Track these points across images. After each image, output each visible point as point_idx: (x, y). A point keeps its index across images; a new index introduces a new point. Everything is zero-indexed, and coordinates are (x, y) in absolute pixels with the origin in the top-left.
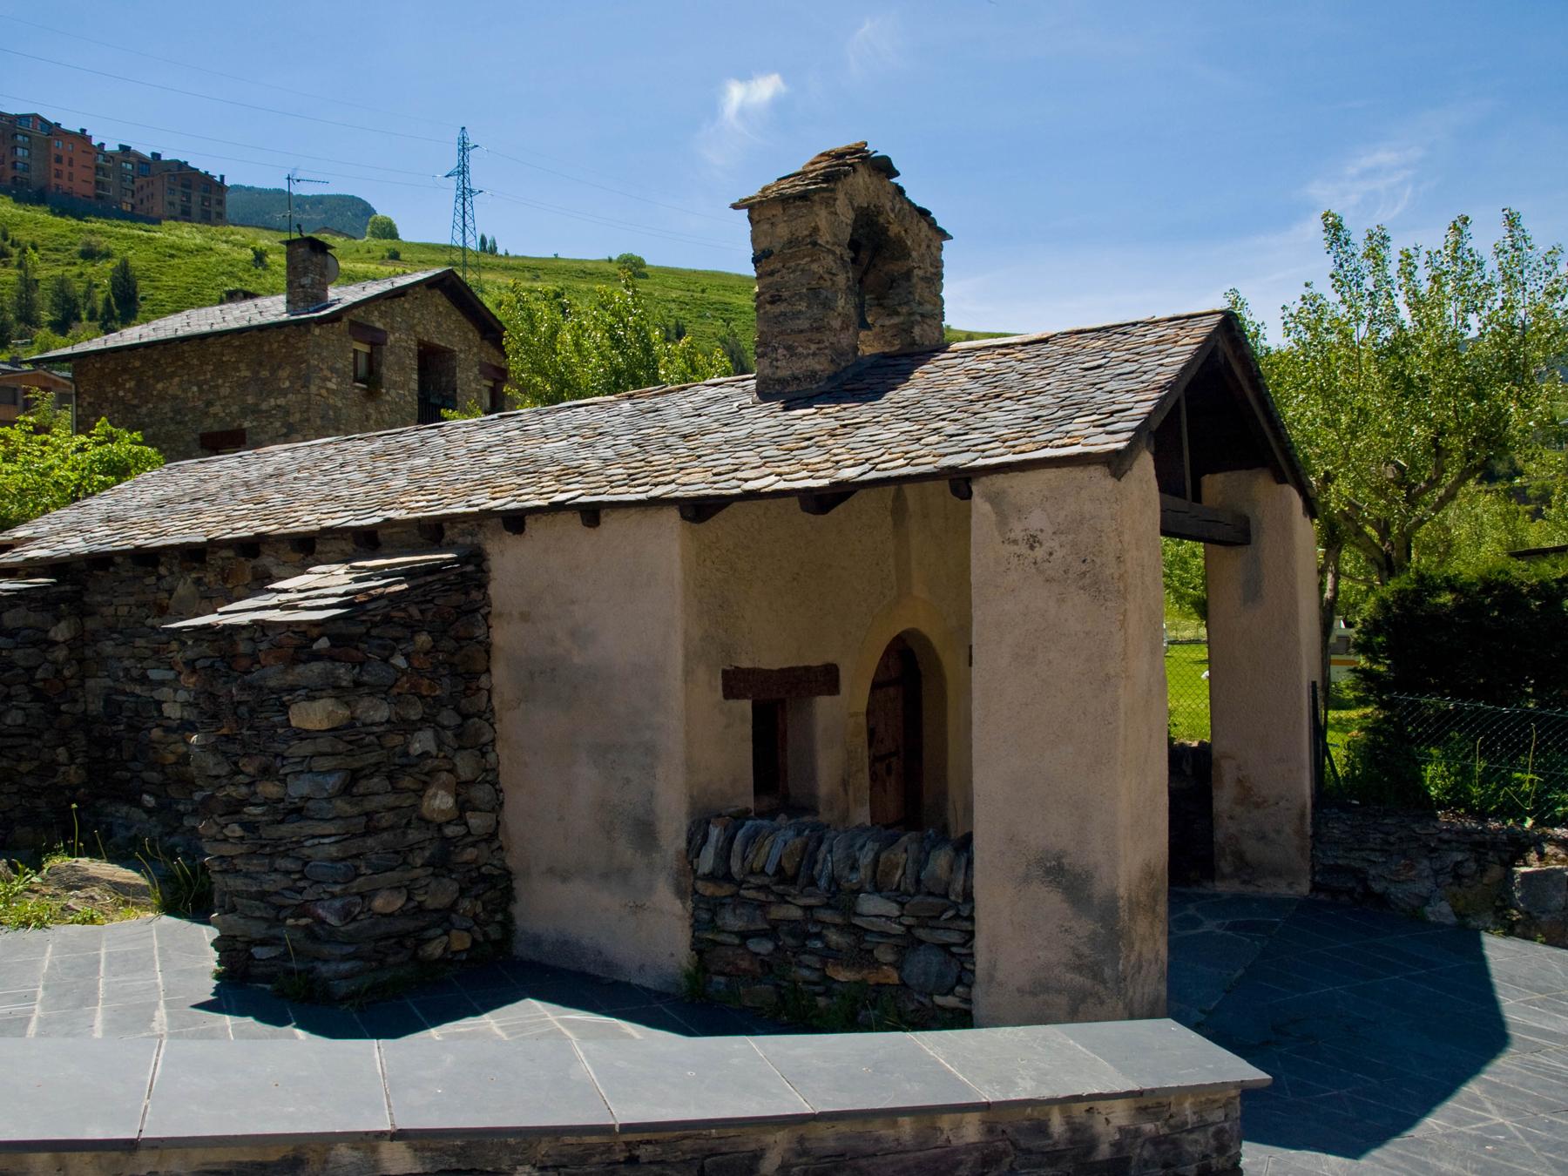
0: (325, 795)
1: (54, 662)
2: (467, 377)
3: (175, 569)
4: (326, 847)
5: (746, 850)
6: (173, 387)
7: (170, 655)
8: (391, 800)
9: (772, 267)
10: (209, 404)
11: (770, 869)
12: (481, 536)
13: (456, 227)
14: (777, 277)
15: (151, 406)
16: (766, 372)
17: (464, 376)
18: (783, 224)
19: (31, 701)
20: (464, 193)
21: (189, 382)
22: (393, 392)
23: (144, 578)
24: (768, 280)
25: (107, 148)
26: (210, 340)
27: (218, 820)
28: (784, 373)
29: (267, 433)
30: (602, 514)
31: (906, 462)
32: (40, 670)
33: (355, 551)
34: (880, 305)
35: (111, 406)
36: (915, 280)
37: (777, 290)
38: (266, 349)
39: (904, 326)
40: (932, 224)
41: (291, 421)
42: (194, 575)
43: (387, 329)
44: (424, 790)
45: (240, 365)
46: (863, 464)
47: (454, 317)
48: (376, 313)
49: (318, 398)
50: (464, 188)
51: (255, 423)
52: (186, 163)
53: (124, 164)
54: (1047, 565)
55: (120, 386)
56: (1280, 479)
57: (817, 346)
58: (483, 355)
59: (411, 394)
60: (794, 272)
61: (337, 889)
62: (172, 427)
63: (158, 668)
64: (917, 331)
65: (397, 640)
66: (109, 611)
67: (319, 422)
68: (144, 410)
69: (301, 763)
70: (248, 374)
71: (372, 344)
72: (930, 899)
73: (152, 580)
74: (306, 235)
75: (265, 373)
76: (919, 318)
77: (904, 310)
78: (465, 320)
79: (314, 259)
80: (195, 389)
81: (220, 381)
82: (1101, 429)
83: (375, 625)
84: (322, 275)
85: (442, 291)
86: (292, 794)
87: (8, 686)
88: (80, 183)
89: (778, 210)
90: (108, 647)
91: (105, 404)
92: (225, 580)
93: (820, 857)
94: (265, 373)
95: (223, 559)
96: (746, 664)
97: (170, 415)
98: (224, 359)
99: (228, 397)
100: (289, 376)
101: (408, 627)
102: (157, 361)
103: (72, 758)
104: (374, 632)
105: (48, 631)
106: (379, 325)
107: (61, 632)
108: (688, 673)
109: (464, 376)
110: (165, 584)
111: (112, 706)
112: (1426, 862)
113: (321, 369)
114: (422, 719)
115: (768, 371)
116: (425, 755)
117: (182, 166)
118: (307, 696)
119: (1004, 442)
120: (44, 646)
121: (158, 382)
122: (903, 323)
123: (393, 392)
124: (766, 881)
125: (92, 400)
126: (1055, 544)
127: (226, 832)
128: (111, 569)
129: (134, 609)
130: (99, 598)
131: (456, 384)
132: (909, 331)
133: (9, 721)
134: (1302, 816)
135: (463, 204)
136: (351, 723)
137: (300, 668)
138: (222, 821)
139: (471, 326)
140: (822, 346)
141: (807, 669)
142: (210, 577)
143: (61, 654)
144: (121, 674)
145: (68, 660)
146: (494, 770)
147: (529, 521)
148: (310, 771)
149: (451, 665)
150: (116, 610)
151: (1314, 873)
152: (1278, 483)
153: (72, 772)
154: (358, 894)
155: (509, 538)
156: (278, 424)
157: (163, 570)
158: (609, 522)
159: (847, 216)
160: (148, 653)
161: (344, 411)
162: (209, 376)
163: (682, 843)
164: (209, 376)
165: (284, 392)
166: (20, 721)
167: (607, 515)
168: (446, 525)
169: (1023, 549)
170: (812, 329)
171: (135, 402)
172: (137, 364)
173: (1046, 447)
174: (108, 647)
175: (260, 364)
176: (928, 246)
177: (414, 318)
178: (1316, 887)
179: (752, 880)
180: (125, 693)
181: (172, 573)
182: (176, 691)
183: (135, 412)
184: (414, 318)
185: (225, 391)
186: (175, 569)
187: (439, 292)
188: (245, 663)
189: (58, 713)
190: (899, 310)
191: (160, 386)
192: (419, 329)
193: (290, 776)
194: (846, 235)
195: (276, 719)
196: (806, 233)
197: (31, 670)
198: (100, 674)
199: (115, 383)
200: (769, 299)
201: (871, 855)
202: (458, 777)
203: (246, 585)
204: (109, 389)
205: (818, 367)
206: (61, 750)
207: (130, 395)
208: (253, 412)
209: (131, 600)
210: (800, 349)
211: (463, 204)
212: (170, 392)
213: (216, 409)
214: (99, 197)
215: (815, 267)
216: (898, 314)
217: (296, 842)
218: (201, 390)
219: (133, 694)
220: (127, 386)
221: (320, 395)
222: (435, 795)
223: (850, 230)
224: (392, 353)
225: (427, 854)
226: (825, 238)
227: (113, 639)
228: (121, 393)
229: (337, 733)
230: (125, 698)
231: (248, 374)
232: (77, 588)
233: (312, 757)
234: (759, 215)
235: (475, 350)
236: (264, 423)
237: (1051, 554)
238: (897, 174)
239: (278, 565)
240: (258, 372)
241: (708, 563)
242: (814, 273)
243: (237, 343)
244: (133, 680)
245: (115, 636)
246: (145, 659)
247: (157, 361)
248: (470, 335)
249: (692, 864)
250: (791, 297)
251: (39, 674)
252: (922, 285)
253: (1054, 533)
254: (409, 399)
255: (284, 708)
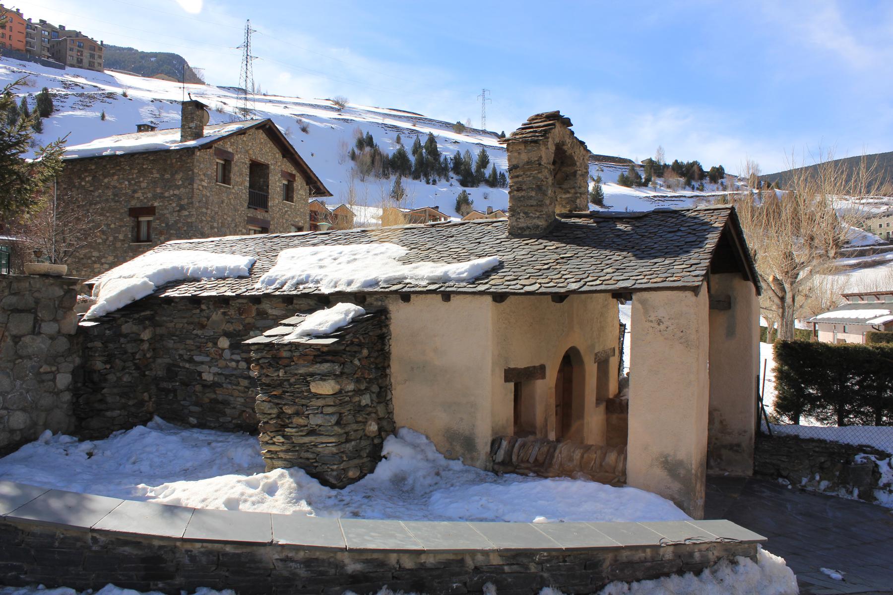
0: (330, 424)
1: (143, 350)
2: (275, 179)
3: (211, 307)
4: (330, 448)
5: (520, 450)
6: (114, 181)
7: (207, 349)
8: (355, 426)
9: (518, 173)
10: (135, 191)
11: (532, 460)
12: (387, 302)
13: (242, 78)
14: (520, 179)
15: (100, 191)
16: (514, 224)
17: (273, 178)
18: (524, 154)
19: (134, 370)
20: (247, 58)
21: (123, 179)
22: (236, 188)
23: (192, 310)
24: (516, 180)
25: (33, 21)
26: (137, 156)
27: (269, 434)
28: (522, 224)
29: (168, 209)
30: (452, 296)
31: (601, 282)
32: (138, 354)
33: (316, 304)
34: (560, 188)
35: (78, 190)
36: (578, 176)
37: (520, 185)
38: (169, 162)
39: (573, 199)
40: (585, 148)
41: (182, 203)
42: (222, 310)
43: (234, 152)
44: (366, 422)
45: (153, 171)
46: (580, 281)
47: (269, 146)
48: (229, 143)
49: (198, 191)
50: (247, 55)
51: (161, 204)
52: (80, 32)
53: (43, 32)
54: (665, 332)
55: (83, 179)
56: (746, 279)
57: (539, 213)
58: (283, 166)
59: (245, 189)
60: (529, 177)
61: (335, 467)
62: (113, 204)
63: (200, 355)
64: (578, 201)
65: (355, 352)
66: (171, 325)
67: (198, 204)
68: (96, 194)
69: (318, 409)
70: (158, 176)
71: (225, 160)
72: (607, 474)
73: (198, 311)
74: (194, 98)
75: (167, 176)
76: (579, 195)
77: (573, 191)
78: (275, 147)
79: (197, 113)
80: (127, 183)
81: (141, 179)
82: (688, 273)
83: (347, 346)
84: (201, 122)
85: (263, 131)
86: (312, 423)
87: (125, 362)
88: (17, 41)
89: (522, 147)
90: (170, 344)
91: (73, 189)
92: (241, 314)
93: (556, 455)
94: (167, 176)
95: (239, 303)
96: (512, 366)
97: (112, 197)
98: (144, 167)
99: (145, 188)
100: (181, 178)
101: (360, 346)
102: (105, 166)
103: (150, 398)
104: (348, 349)
105: (140, 335)
106: (230, 150)
107: (146, 335)
108: (493, 371)
109: (273, 178)
110: (204, 314)
111: (171, 371)
112: (807, 461)
113: (200, 175)
114: (365, 389)
115: (515, 224)
116: (367, 405)
117: (78, 34)
118: (321, 378)
119: (645, 276)
120: (139, 342)
121: (105, 178)
122: (571, 198)
123: (236, 188)
124: (529, 465)
125: (65, 186)
126: (669, 323)
127: (275, 440)
128: (173, 304)
129: (186, 325)
130: (165, 318)
131: (268, 183)
132: (574, 202)
133: (125, 380)
134: (751, 438)
135: (246, 65)
136: (340, 392)
137: (318, 366)
138: (272, 435)
139: (278, 151)
140: (542, 213)
141: (534, 367)
142: (232, 312)
143: (146, 346)
144: (177, 357)
145: (148, 350)
146: (391, 412)
147: (413, 296)
148: (322, 413)
149: (376, 364)
150: (175, 325)
151: (755, 466)
152: (745, 280)
153: (151, 405)
154: (343, 469)
155: (402, 304)
156: (174, 205)
157: (203, 307)
158: (455, 299)
159: (552, 148)
160: (193, 348)
161: (211, 198)
162: (135, 176)
163: (488, 449)
164: (135, 176)
165: (178, 187)
166: (129, 380)
167: (454, 297)
168: (367, 296)
169: (655, 325)
170: (537, 205)
171: (91, 189)
172: (93, 167)
173: (665, 281)
174: (170, 344)
175: (165, 170)
176: (583, 159)
177: (248, 146)
178: (755, 473)
179: (523, 465)
180: (180, 367)
181: (209, 308)
182: (210, 367)
183: (91, 194)
184: (248, 146)
185: (144, 185)
186: (211, 307)
187: (262, 132)
188: (286, 362)
189: (145, 375)
190: (570, 191)
191: (106, 180)
192: (251, 152)
193: (311, 415)
194: (551, 160)
195: (303, 388)
196: (536, 159)
197: (134, 354)
198: (165, 356)
199: (80, 178)
200: (516, 189)
201: (580, 454)
202: (378, 415)
203: (253, 317)
204: (77, 181)
205: (540, 223)
206: (146, 394)
207: (88, 185)
208: (160, 197)
209: (185, 321)
210: (531, 214)
211: (246, 65)
212: (112, 184)
213: (139, 195)
214: (27, 51)
215: (540, 175)
216: (569, 192)
217: (314, 445)
218: (130, 184)
219: (184, 368)
220: (87, 179)
221: (199, 189)
222: (370, 425)
223: (553, 155)
224: (236, 165)
225: (367, 451)
226: (544, 161)
227: (173, 339)
228: (83, 183)
229: (336, 396)
230: (179, 369)
231: (158, 176)
232: (152, 313)
233: (323, 407)
234: (512, 148)
235: (279, 164)
236: (166, 204)
237: (667, 328)
238: (572, 125)
239: (272, 308)
240: (164, 175)
241: (501, 320)
242: (539, 178)
243: (152, 158)
244: (184, 360)
245: (174, 338)
246: (193, 350)
247: (105, 166)
248: (277, 156)
249: (492, 457)
250: (527, 189)
251: (137, 357)
252: (581, 178)
253: (669, 319)
254: (244, 191)
255: (308, 384)
